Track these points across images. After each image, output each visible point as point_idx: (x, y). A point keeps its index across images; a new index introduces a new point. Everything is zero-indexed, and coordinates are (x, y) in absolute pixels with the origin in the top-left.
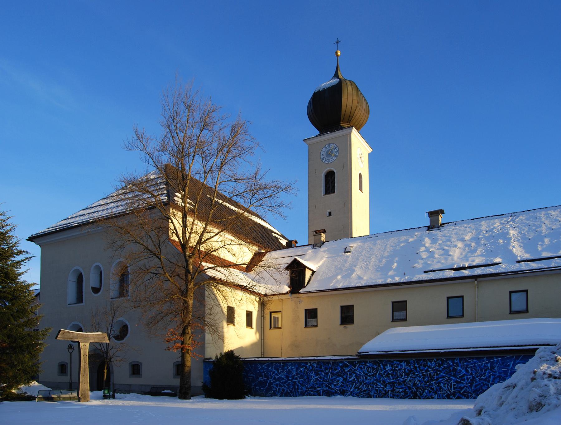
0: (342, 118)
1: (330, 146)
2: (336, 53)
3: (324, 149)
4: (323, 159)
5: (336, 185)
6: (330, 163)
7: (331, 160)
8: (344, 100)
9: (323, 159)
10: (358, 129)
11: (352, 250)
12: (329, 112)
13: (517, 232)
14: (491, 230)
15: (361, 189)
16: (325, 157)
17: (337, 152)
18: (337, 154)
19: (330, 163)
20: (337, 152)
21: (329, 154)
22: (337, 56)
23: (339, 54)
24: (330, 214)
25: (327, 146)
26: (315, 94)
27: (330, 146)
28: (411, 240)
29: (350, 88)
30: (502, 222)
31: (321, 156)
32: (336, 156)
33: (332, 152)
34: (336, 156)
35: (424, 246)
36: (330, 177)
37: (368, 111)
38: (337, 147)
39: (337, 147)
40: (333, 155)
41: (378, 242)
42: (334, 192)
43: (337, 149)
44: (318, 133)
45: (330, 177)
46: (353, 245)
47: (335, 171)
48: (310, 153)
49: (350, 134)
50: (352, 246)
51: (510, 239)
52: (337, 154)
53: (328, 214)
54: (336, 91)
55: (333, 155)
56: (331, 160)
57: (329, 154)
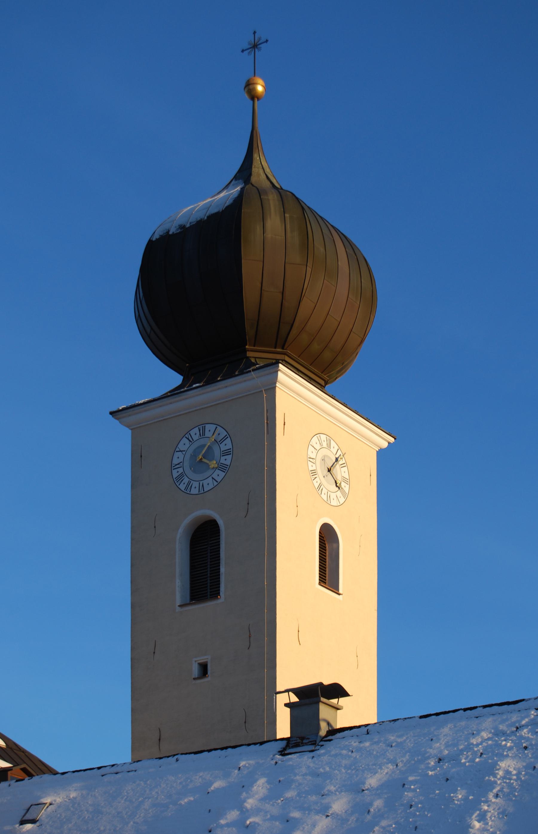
0: (250, 332)
1: (202, 434)
2: (249, 87)
3: (184, 445)
4: (180, 477)
5: (222, 570)
6: (202, 492)
7: (209, 484)
8: (250, 269)
9: (180, 477)
10: (322, 372)
11: (43, 814)
12: (215, 309)
17: (226, 453)
18: (227, 460)
19: (202, 492)
20: (226, 453)
21: (199, 464)
22: (253, 96)
23: (260, 88)
24: (204, 669)
26: (152, 248)
27: (202, 434)
28: (218, 784)
30: (502, 727)
31: (173, 467)
32: (222, 467)
34: (222, 467)
35: (241, 807)
36: (205, 539)
37: (370, 300)
39: (228, 435)
40: (213, 464)
41: (199, 784)
42: (215, 594)
43: (227, 445)
44: (177, 379)
45: (205, 539)
46: (54, 798)
47: (220, 522)
48: (138, 458)
49: (271, 390)
52: (227, 460)
53: (195, 670)
55: (213, 464)
56: (209, 484)
57: (199, 464)
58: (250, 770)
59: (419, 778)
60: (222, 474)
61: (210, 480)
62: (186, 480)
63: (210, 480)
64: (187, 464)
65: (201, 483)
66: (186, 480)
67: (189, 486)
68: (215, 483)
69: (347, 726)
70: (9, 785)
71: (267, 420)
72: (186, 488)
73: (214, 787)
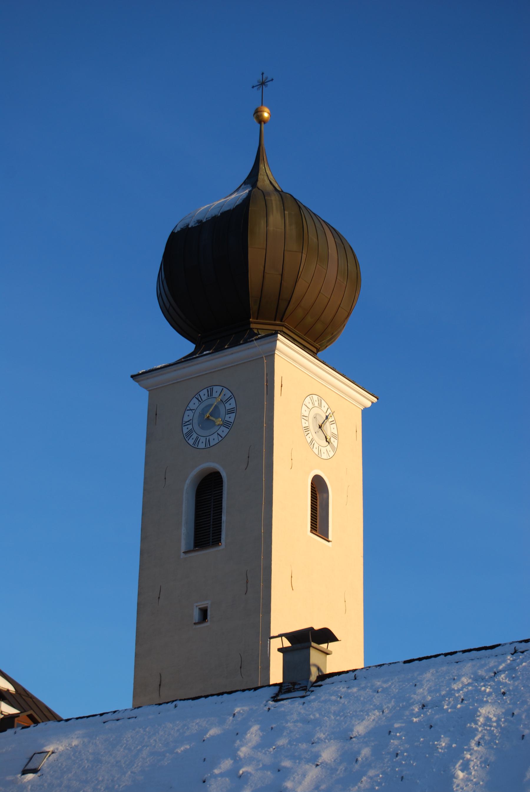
0: (254, 307)
1: (210, 395)
2: (257, 114)
3: (194, 404)
5: (224, 518)
6: (208, 446)
7: (214, 439)
10: (315, 340)
12: (225, 289)
13: (499, 711)
14: (437, 704)
15: (319, 523)
16: (197, 428)
18: (230, 418)
19: (208, 446)
22: (261, 121)
23: (266, 115)
25: (204, 394)
26: (174, 238)
27: (210, 395)
28: (213, 732)
29: (276, 218)
30: (481, 672)
32: (226, 424)
33: (215, 412)
34: (226, 424)
36: (209, 490)
38: (233, 396)
39: (233, 396)
40: (219, 421)
41: (195, 731)
42: (217, 541)
43: (232, 404)
44: (190, 347)
45: (209, 490)
48: (153, 416)
49: (271, 356)
50: (50, 748)
51: (473, 732)
52: (230, 418)
53: (196, 615)
54: (229, 230)
55: (219, 421)
56: (214, 439)
57: (206, 422)
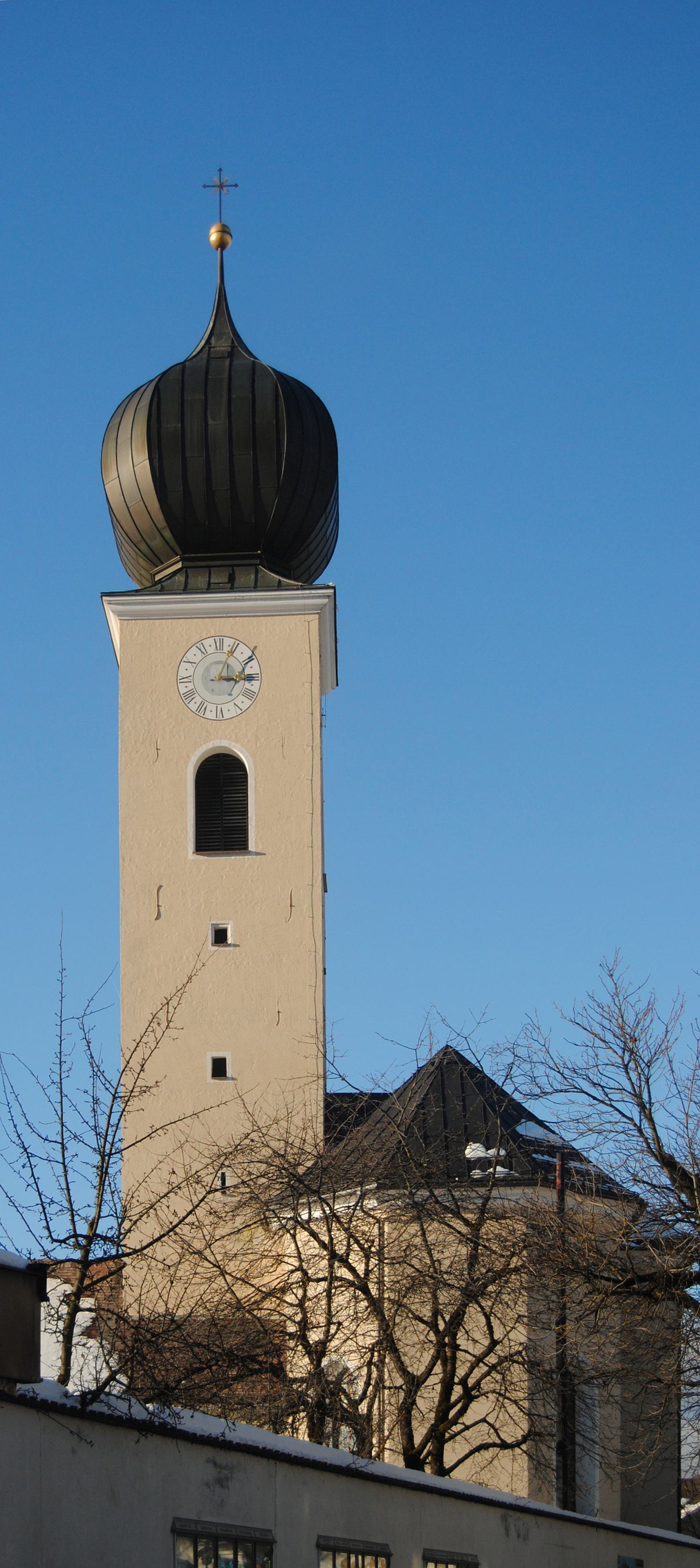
3: (194, 655)
19: (220, 717)
31: (180, 680)
56: (230, 711)
58: (555, 1498)
59: (422, 1457)
60: (248, 702)
61: (231, 706)
62: (198, 700)
63: (231, 706)
64: (198, 679)
65: (219, 707)
66: (198, 700)
67: (202, 707)
68: (239, 712)
69: (185, 1517)
70: (192, 1417)
71: (279, 454)
72: (199, 709)
73: (488, 1149)
